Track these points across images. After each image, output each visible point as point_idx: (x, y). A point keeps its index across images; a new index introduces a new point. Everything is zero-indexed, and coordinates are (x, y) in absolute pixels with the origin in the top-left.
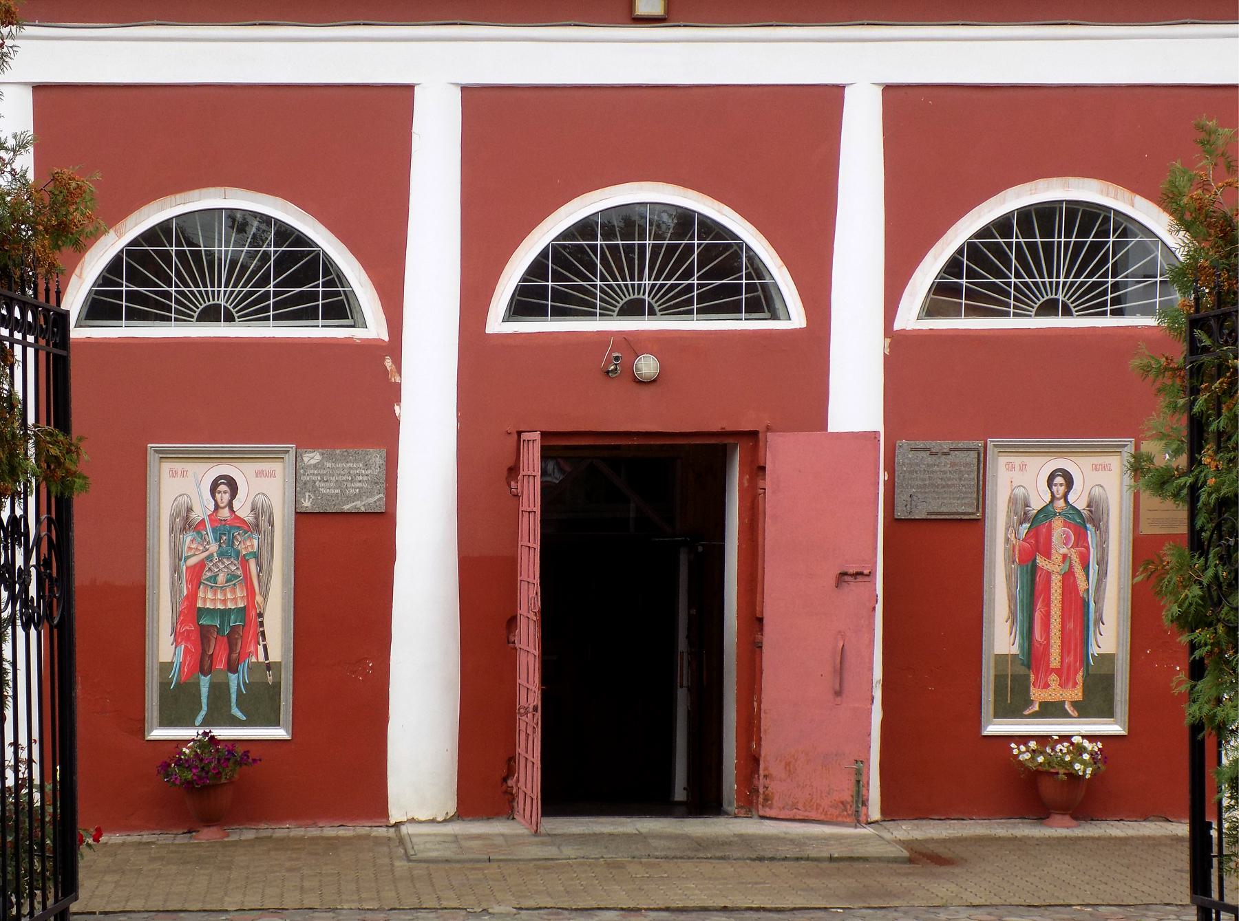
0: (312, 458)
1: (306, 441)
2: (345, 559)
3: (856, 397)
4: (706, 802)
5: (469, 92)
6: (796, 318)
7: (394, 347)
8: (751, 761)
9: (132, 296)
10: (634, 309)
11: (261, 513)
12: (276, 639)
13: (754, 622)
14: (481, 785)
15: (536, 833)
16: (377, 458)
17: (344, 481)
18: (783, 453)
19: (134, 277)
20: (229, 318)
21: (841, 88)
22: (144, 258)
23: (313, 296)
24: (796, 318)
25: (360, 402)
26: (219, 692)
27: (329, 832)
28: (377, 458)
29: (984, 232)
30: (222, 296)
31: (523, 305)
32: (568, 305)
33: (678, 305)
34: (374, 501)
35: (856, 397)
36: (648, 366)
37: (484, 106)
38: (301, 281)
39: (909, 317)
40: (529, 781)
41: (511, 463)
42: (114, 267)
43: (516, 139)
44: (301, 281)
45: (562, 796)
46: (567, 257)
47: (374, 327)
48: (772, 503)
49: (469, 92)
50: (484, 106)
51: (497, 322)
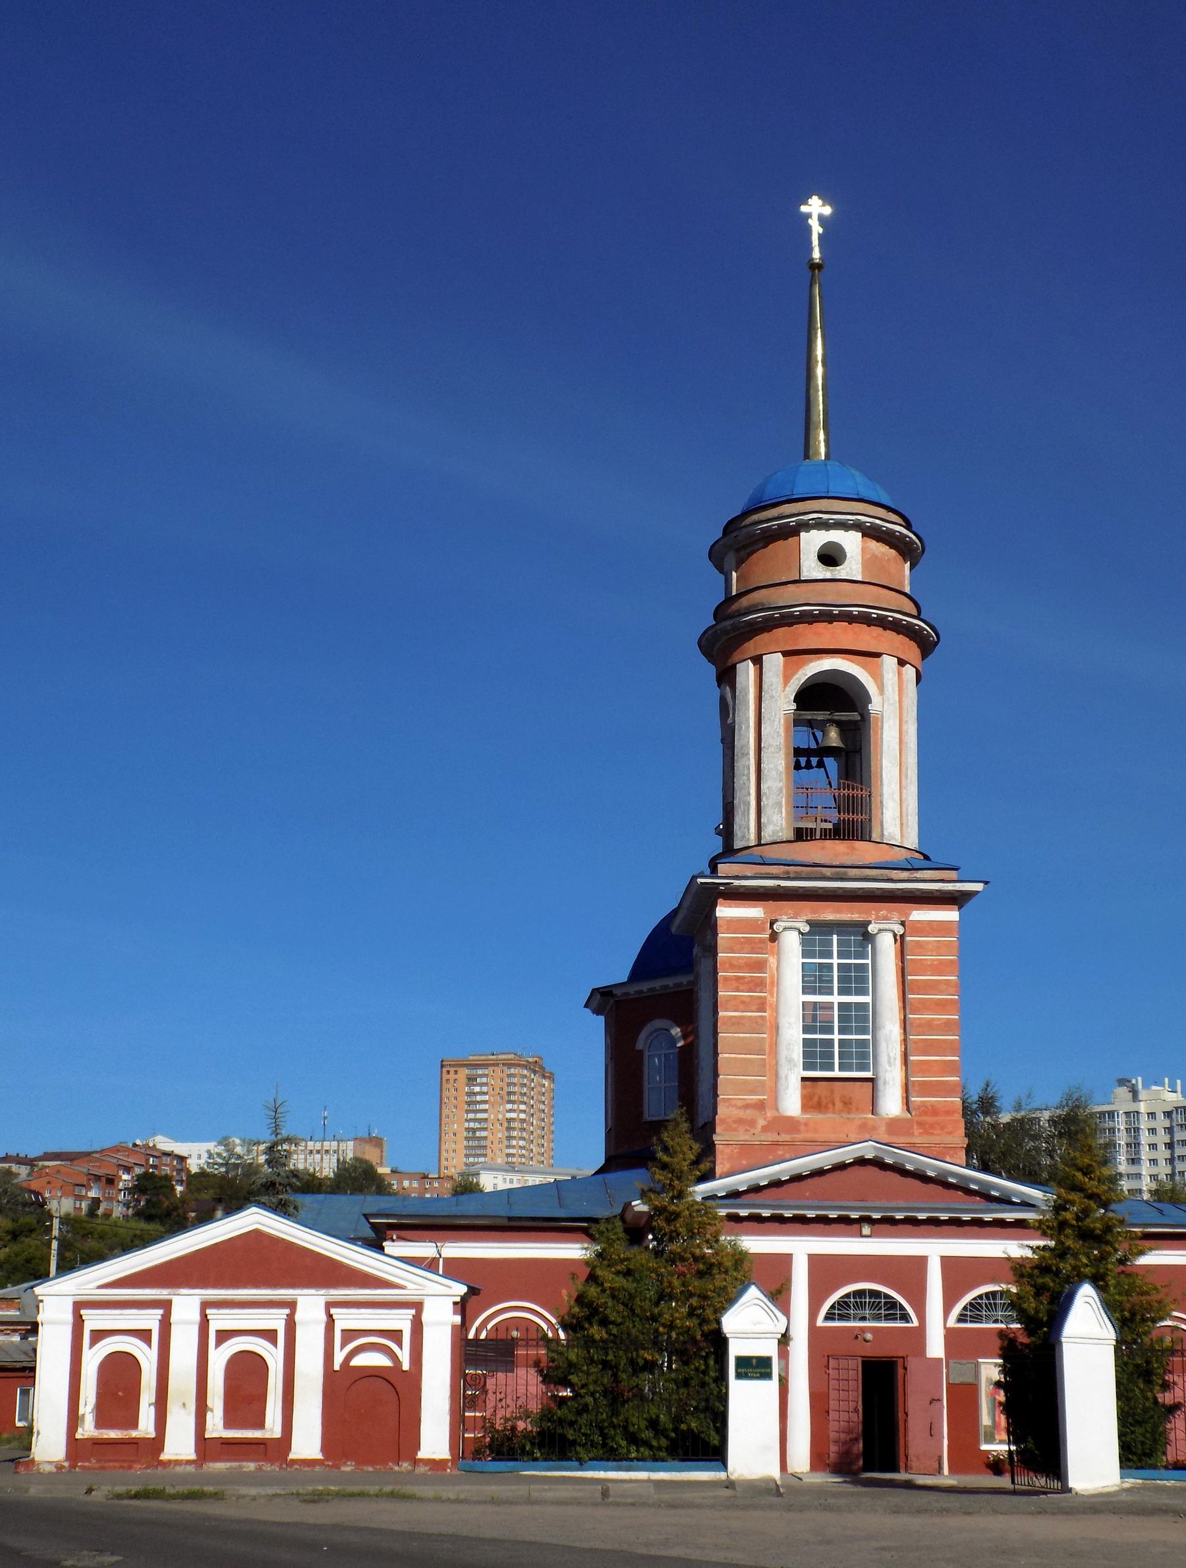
3: (936, 1347)
10: (863, 1319)
15: (418, 1306)
18: (912, 1364)
22: (845, 1302)
31: (829, 1317)
32: (842, 1317)
33: (877, 1318)
35: (936, 1347)
36: (869, 1336)
39: (952, 1322)
46: (843, 1304)
50: (815, 1261)
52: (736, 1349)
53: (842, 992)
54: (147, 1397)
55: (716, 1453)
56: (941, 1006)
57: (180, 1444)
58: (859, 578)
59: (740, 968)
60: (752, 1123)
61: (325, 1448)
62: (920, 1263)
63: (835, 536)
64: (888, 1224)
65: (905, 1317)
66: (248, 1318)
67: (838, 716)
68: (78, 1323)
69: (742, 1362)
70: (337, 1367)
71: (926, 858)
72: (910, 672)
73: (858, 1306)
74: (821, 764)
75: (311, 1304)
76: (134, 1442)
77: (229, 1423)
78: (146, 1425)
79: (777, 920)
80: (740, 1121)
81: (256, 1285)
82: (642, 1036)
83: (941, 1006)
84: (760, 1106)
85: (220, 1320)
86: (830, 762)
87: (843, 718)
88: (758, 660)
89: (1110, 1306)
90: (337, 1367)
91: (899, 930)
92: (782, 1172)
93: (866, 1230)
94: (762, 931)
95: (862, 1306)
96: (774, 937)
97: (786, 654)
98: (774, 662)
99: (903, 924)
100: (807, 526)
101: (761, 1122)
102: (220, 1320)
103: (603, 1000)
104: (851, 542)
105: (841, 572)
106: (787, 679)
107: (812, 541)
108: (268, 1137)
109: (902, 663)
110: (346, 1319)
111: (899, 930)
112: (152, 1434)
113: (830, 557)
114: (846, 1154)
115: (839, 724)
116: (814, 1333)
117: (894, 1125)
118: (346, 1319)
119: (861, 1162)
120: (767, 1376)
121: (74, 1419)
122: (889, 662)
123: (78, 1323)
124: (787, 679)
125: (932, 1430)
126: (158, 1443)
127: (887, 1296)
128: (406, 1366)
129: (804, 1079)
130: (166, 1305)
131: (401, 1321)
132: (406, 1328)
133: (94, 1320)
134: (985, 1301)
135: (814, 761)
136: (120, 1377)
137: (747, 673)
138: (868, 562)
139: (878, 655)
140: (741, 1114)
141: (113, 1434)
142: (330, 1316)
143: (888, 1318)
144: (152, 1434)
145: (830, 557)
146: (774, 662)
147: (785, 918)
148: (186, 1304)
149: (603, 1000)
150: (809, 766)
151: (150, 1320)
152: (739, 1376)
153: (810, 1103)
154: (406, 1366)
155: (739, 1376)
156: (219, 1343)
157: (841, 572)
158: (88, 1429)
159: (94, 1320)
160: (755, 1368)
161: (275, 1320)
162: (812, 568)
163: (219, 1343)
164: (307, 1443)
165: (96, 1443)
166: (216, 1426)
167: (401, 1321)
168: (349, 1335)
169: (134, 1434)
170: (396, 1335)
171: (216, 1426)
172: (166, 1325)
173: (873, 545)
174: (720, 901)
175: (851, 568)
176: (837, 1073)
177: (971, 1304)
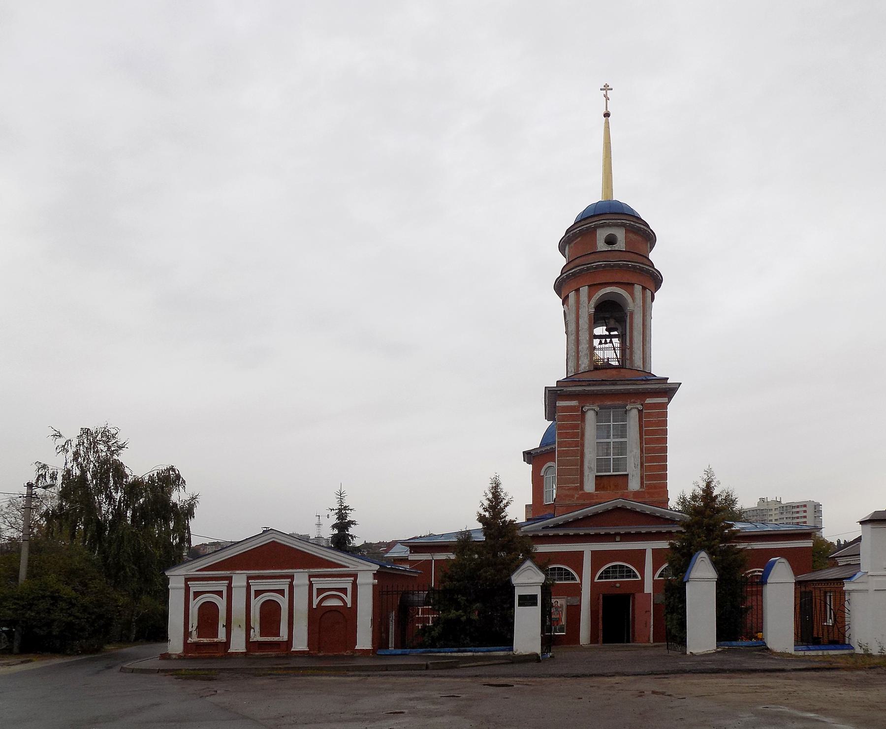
1: (568, 596)
2: (574, 612)
3: (648, 588)
4: (628, 642)
6: (640, 578)
7: (581, 583)
8: (633, 635)
10: (616, 578)
11: (562, 606)
12: (563, 622)
13: (634, 617)
14: (594, 638)
15: (355, 576)
17: (574, 601)
18: (637, 595)
24: (640, 578)
25: (577, 590)
26: (555, 629)
31: (600, 578)
32: (606, 578)
33: (622, 577)
35: (648, 588)
36: (618, 585)
37: (594, 553)
39: (656, 578)
40: (601, 639)
41: (604, 111)
43: (598, 558)
45: (604, 642)
46: (606, 571)
47: (578, 581)
48: (636, 602)
50: (594, 553)
52: (518, 592)
54: (222, 621)
55: (508, 641)
57: (238, 645)
59: (568, 428)
60: (573, 496)
61: (309, 645)
64: (627, 537)
65: (574, 579)
66: (271, 585)
68: (187, 589)
69: (521, 597)
70: (314, 607)
73: (613, 572)
74: (611, 342)
75: (301, 578)
76: (217, 644)
77: (262, 634)
78: (222, 636)
80: (567, 496)
81: (254, 569)
82: (543, 470)
84: (576, 488)
85: (256, 586)
86: (615, 340)
88: (577, 290)
89: (715, 564)
90: (314, 607)
91: (640, 407)
94: (578, 411)
96: (583, 413)
98: (584, 290)
100: (603, 226)
101: (576, 496)
102: (256, 586)
103: (529, 456)
105: (616, 247)
108: (337, 506)
110: (318, 583)
111: (640, 407)
112: (286, 638)
113: (611, 240)
117: (636, 494)
118: (318, 583)
120: (535, 604)
121: (187, 634)
123: (187, 589)
125: (647, 624)
126: (227, 644)
128: (349, 605)
130: (230, 579)
131: (347, 583)
132: (349, 587)
133: (195, 587)
135: (608, 340)
136: (208, 614)
140: (567, 492)
141: (205, 640)
142: (311, 582)
144: (286, 638)
145: (611, 240)
148: (239, 579)
149: (529, 456)
150: (606, 343)
151: (222, 586)
152: (520, 605)
153: (598, 487)
154: (349, 605)
155: (520, 605)
156: (195, 597)
157: (616, 247)
158: (194, 639)
159: (195, 587)
161: (284, 585)
162: (601, 246)
163: (195, 597)
164: (300, 643)
165: (197, 645)
166: (255, 636)
167: (347, 583)
168: (320, 591)
169: (215, 640)
170: (344, 591)
171: (255, 636)
172: (230, 588)
175: (621, 245)
176: (612, 473)
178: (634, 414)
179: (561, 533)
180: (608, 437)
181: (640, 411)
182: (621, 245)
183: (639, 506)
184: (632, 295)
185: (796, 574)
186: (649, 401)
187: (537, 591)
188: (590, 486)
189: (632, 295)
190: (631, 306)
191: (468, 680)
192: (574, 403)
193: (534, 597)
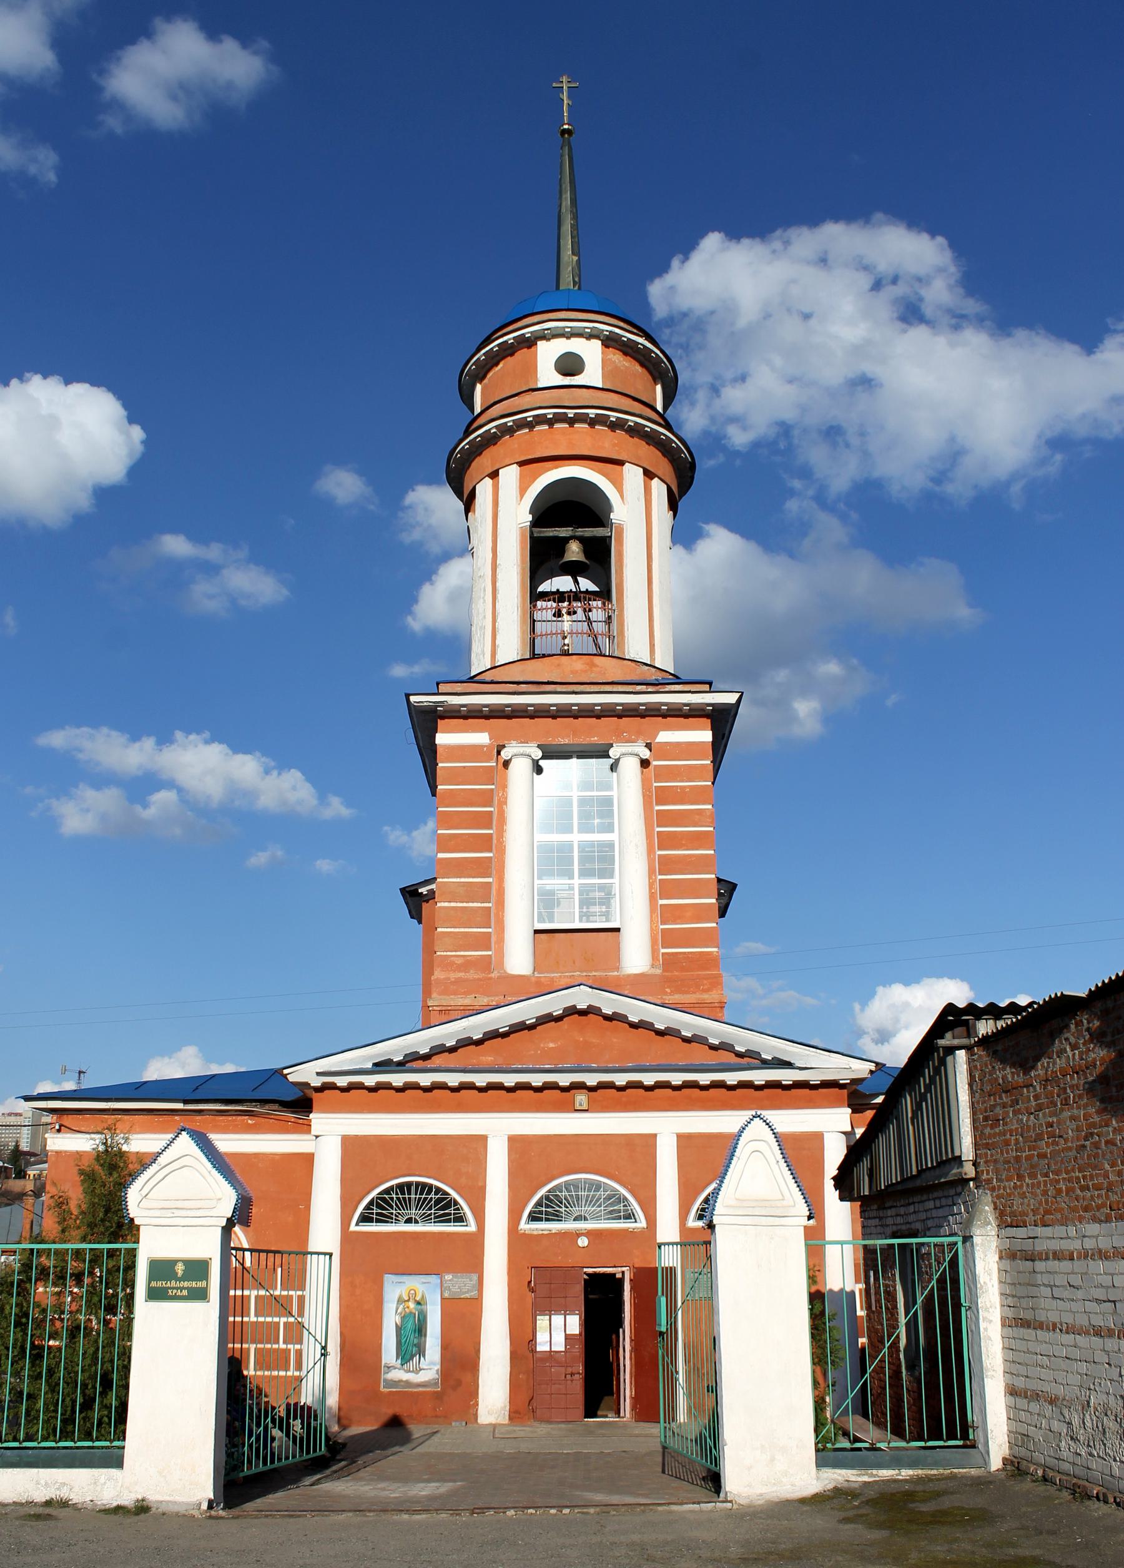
0: (448, 1277)
2: (463, 1319)
5: (680, 1137)
6: (472, 1227)
9: (377, 1214)
16: (475, 1277)
19: (379, 1206)
20: (416, 1222)
21: (655, 1136)
22: (383, 1200)
23: (450, 1214)
25: (469, 1255)
27: (906, 1473)
28: (475, 1277)
29: (549, 1191)
30: (584, 1209)
32: (383, 1219)
33: (426, 1219)
34: (474, 1293)
37: (518, 1145)
38: (446, 1210)
42: (371, 1203)
44: (446, 1210)
46: (382, 1202)
49: (680, 1137)
50: (518, 1145)
51: (353, 1227)
52: (151, 1246)
53: (581, 830)
56: (697, 840)
58: (600, 386)
62: (649, 1142)
63: (577, 346)
64: (606, 1096)
65: (460, 1219)
67: (580, 532)
69: (161, 1269)
71: (678, 678)
72: (659, 489)
79: (504, 746)
83: (697, 840)
87: (587, 534)
88: (494, 475)
91: (646, 754)
92: (474, 1027)
93: (581, 1098)
95: (405, 1203)
97: (521, 464)
98: (510, 475)
99: (648, 746)
100: (544, 336)
104: (591, 352)
106: (523, 491)
107: (548, 353)
109: (649, 474)
111: (646, 754)
113: (570, 365)
114: (554, 1004)
115: (582, 540)
116: (516, 1239)
119: (572, 1011)
120: (201, 1295)
122: (632, 474)
124: (523, 491)
127: (438, 1190)
129: (536, 932)
134: (565, 1193)
137: (484, 489)
138: (608, 369)
139: (621, 463)
143: (444, 1219)
145: (570, 365)
146: (510, 475)
147: (514, 743)
153: (539, 958)
155: (154, 1295)
160: (178, 1280)
162: (547, 375)
173: (616, 357)
174: (441, 723)
175: (592, 375)
177: (547, 1198)
178: (630, 767)
179: (398, 1079)
180: (569, 830)
181: (645, 763)
182: (592, 375)
183: (636, 1010)
184: (618, 485)
185: (865, 1236)
186: (665, 737)
187: (208, 1247)
188: (518, 958)
189: (618, 485)
190: (618, 514)
191: (350, 1514)
192: (480, 738)
193: (198, 1268)
